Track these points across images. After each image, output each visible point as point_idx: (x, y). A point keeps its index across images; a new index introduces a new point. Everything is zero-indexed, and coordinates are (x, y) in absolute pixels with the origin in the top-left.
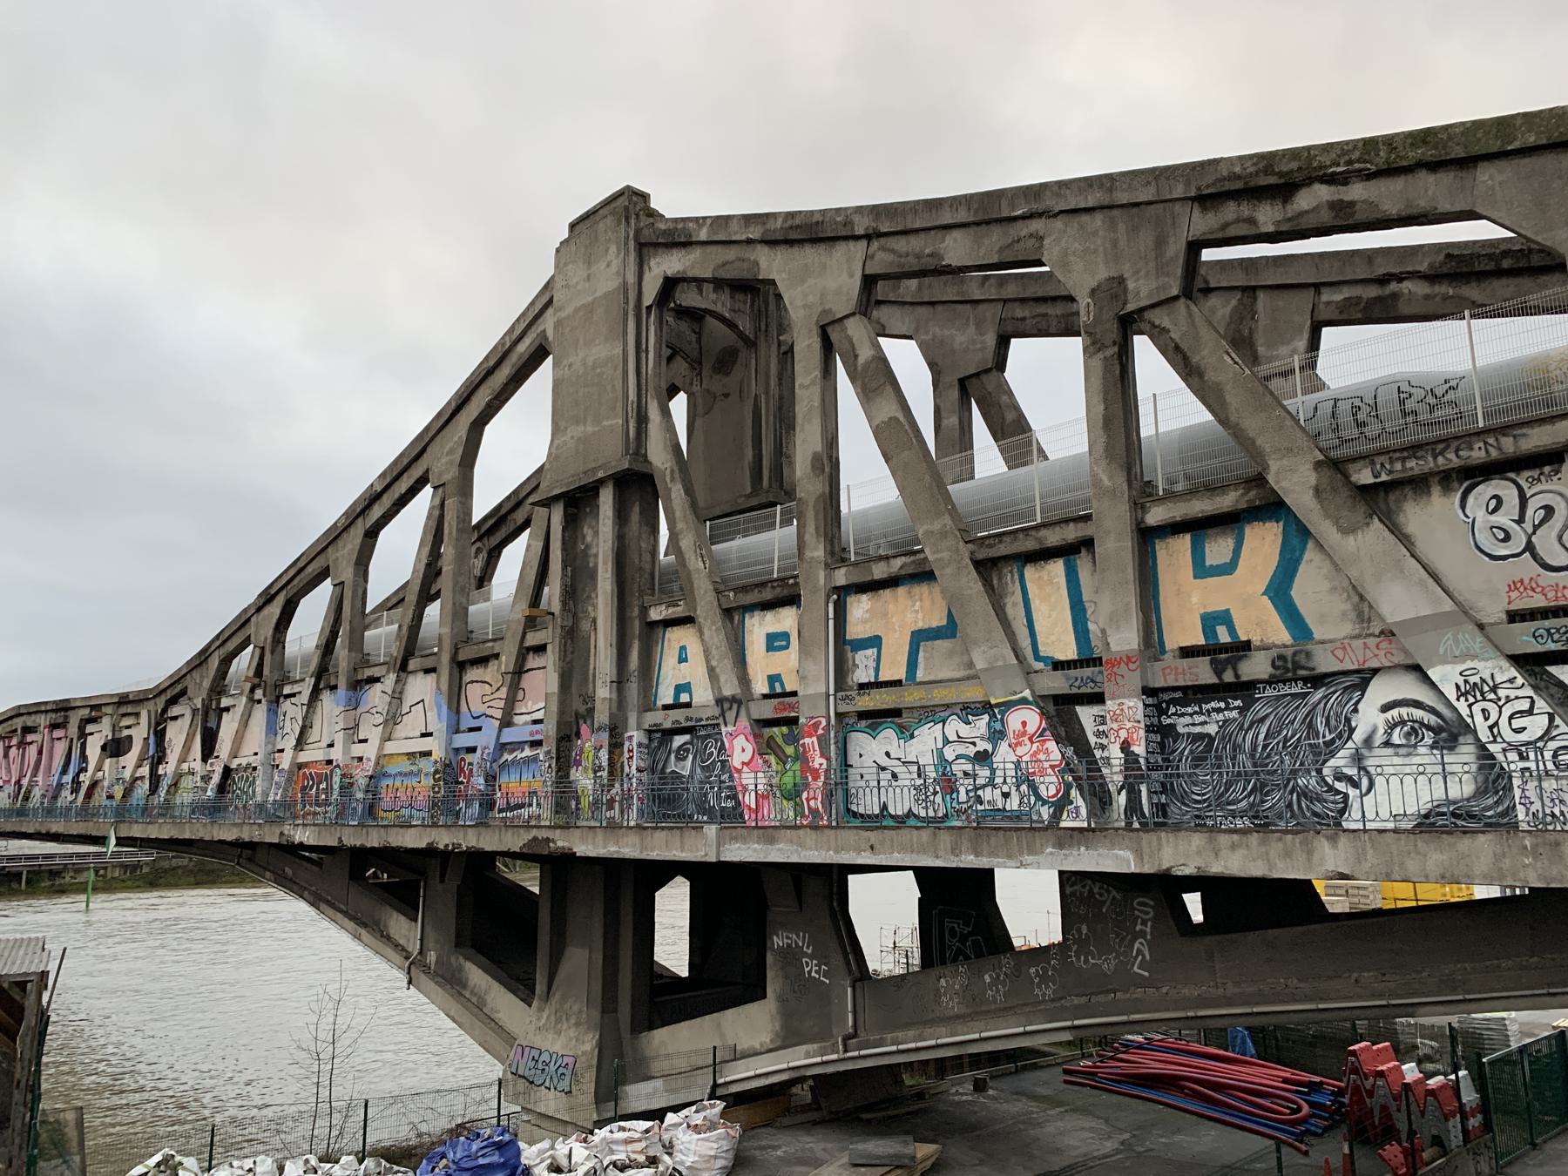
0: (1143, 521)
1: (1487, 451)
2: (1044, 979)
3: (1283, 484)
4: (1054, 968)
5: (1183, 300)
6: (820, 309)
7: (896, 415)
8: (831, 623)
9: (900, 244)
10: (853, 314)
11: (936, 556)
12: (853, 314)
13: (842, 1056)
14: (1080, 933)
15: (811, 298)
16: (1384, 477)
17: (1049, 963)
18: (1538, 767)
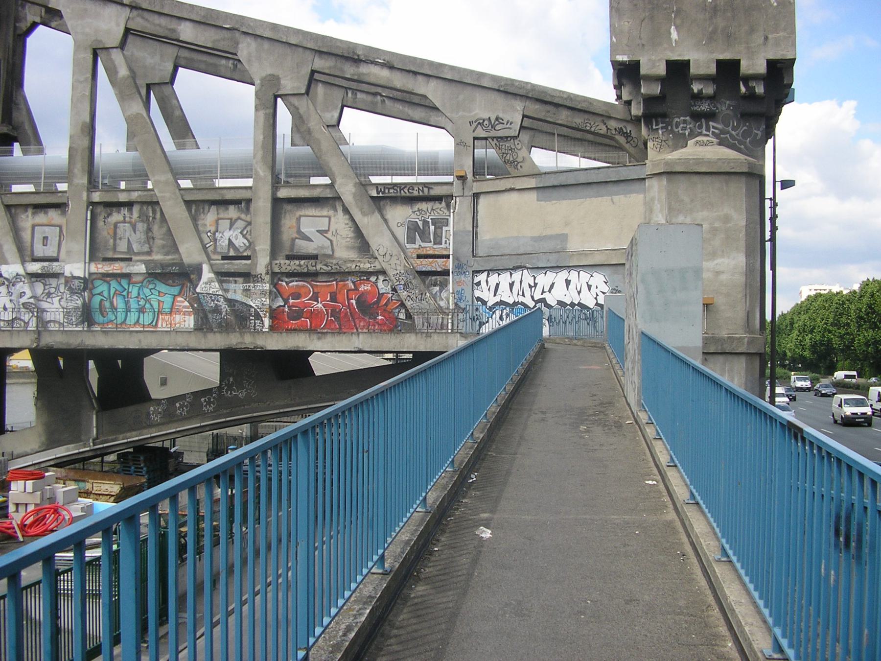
0: (276, 194)
1: (419, 192)
2: (209, 403)
3: (341, 190)
4: (214, 398)
5: (306, 96)
6: (93, 38)
7: (141, 112)
8: (89, 222)
9: (157, 20)
10: (116, 48)
11: (162, 194)
12: (116, 48)
13: (92, 448)
14: (229, 381)
15: (87, 30)
16: (381, 195)
17: (212, 396)
18: (55, 614)
